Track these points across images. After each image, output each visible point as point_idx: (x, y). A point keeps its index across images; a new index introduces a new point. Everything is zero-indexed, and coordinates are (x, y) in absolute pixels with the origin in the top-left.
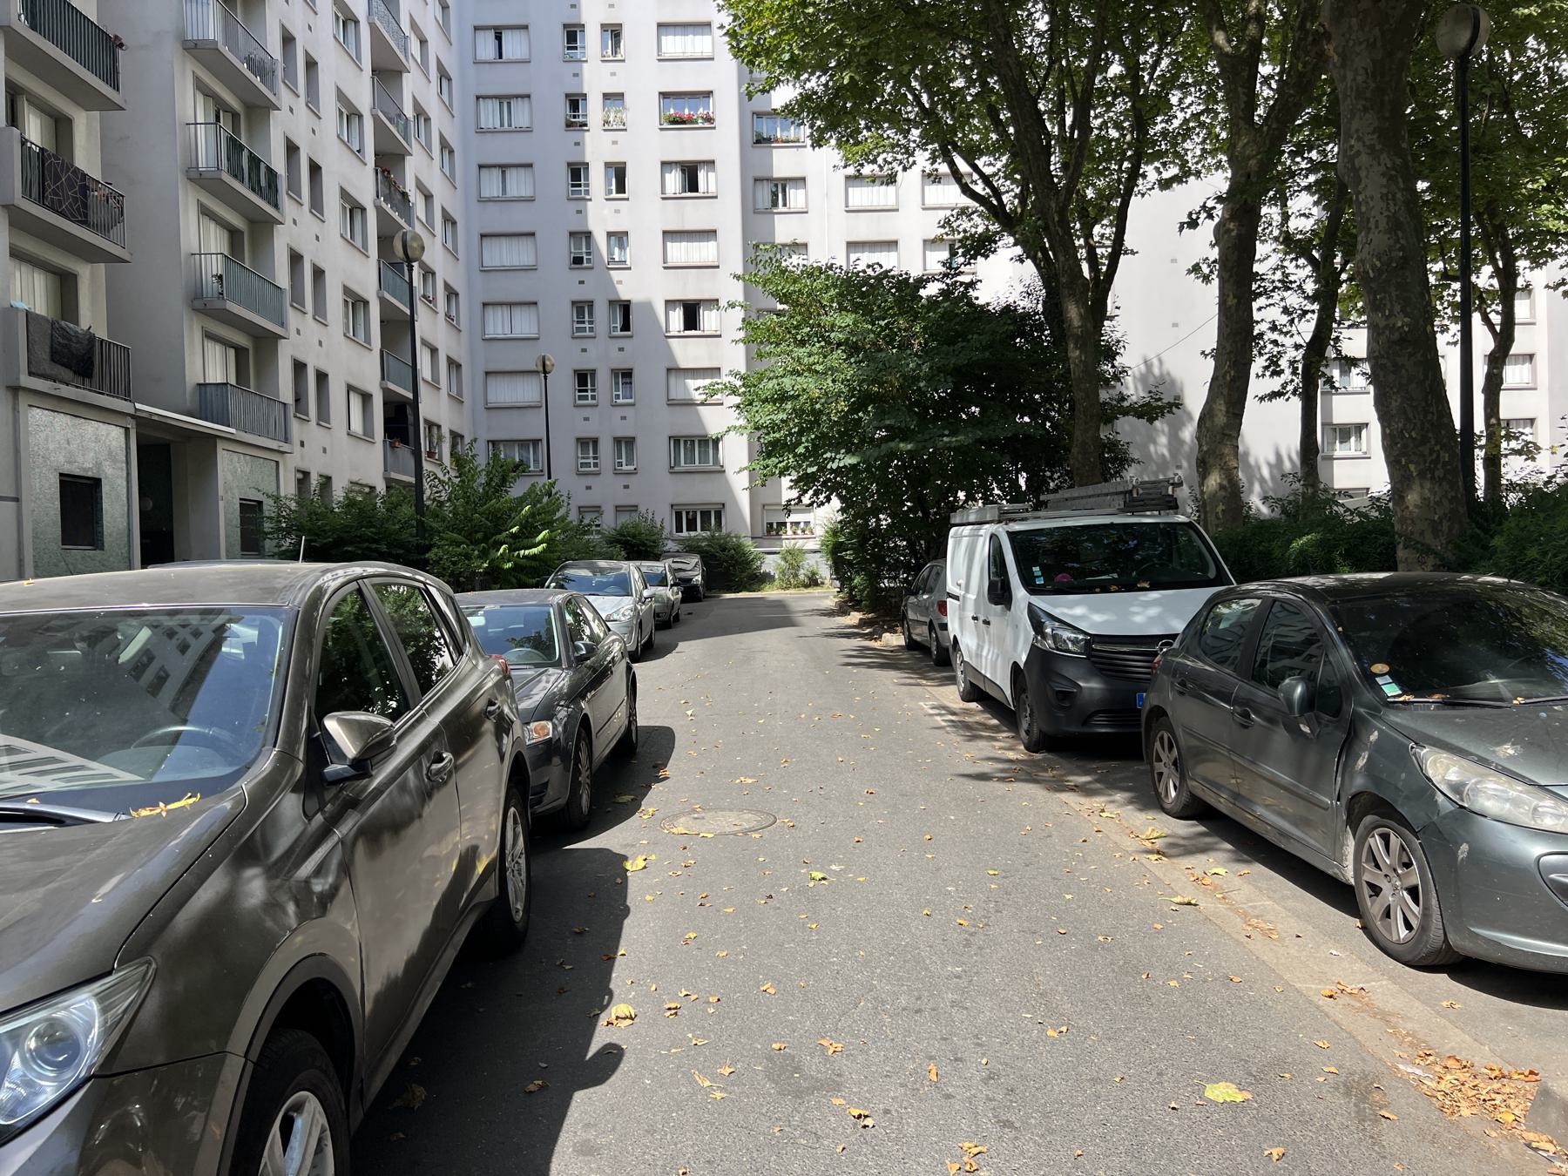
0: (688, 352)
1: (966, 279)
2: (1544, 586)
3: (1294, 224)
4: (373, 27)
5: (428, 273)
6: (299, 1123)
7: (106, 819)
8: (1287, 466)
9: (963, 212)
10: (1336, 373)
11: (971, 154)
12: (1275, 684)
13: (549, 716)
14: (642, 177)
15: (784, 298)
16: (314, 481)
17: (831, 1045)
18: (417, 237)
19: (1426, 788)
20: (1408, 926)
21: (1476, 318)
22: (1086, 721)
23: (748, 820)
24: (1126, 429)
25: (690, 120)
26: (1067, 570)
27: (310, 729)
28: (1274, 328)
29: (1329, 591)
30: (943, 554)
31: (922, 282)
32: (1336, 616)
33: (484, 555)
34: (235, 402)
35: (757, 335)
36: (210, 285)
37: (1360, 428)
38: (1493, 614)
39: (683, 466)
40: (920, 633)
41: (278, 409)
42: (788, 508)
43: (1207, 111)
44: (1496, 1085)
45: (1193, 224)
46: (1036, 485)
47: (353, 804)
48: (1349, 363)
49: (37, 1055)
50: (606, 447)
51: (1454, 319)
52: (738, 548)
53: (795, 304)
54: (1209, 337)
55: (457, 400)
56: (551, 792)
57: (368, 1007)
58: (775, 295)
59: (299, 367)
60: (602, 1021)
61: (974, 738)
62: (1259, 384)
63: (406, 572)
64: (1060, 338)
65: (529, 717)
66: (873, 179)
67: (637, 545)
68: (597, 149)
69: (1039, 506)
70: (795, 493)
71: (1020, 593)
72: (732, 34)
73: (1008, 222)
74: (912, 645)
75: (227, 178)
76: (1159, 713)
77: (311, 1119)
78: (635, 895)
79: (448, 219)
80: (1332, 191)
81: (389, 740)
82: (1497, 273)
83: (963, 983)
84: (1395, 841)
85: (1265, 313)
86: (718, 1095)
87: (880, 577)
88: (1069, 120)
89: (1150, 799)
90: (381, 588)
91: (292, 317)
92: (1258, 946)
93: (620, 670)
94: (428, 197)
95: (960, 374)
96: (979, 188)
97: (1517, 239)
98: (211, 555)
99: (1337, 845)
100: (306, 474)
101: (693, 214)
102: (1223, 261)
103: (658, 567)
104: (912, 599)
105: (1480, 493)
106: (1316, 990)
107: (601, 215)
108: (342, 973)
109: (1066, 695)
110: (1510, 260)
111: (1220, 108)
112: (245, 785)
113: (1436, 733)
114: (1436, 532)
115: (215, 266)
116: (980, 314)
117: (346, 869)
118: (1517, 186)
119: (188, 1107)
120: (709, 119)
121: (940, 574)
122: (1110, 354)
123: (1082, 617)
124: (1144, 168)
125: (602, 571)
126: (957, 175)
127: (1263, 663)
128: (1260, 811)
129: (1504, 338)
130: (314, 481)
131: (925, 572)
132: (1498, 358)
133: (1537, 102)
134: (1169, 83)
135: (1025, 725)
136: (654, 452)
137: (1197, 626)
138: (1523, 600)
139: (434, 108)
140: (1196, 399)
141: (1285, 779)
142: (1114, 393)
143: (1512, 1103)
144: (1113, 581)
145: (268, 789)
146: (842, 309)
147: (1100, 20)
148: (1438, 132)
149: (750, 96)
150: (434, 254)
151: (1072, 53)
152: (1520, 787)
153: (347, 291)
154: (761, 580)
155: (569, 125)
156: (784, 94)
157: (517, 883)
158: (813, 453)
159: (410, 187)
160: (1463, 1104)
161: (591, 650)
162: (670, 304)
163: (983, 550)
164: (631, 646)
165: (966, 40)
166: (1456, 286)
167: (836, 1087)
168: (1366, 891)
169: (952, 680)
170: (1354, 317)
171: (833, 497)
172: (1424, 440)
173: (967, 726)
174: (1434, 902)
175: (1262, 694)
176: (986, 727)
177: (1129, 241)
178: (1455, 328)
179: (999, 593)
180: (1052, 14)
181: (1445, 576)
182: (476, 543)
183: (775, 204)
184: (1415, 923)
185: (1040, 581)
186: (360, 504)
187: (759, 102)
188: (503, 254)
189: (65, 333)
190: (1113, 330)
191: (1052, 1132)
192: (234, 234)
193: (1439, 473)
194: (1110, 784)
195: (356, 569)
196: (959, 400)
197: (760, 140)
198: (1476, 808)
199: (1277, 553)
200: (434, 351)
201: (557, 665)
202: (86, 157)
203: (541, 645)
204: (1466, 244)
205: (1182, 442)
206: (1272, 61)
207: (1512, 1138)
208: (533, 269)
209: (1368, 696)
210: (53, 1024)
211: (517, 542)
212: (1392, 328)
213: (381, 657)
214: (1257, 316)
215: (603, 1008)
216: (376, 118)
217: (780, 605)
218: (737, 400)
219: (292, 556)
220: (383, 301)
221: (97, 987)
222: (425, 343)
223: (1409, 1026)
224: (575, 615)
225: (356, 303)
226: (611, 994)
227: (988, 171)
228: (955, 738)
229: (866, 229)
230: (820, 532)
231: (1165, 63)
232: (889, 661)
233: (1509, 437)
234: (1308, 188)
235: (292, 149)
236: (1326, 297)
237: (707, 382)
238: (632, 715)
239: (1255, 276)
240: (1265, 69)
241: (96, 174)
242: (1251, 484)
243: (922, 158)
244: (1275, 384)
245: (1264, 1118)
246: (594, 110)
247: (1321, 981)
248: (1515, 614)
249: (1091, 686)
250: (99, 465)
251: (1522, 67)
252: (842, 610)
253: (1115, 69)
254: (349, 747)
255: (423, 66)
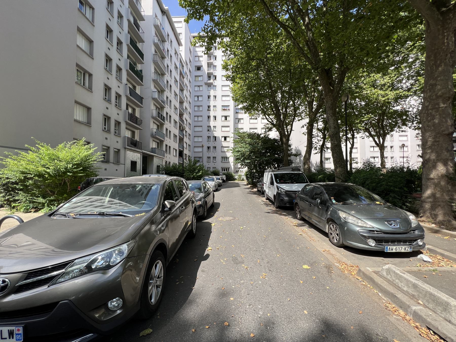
0: (224, 144)
1: (268, 134)
2: (359, 185)
3: (319, 127)
4: (180, 96)
5: (186, 132)
6: (158, 265)
7: (131, 216)
8: (318, 164)
9: (267, 124)
10: (326, 150)
11: (269, 115)
12: (316, 199)
13: (200, 201)
14: (218, 118)
15: (240, 136)
16: (168, 162)
17: (243, 256)
18: (184, 127)
19: (340, 218)
20: (337, 240)
21: (348, 142)
22: (285, 204)
23: (231, 218)
24: (292, 158)
25: (226, 110)
26: (283, 180)
27: (163, 203)
28: (316, 143)
29: (324, 185)
30: (263, 176)
31: (261, 134)
32: (325, 189)
33: (192, 174)
34: (157, 151)
35: (235, 142)
36: (154, 133)
37: (329, 158)
38: (351, 190)
39: (223, 161)
40: (260, 189)
41: (163, 151)
42: (239, 168)
43: (306, 109)
44: (351, 268)
45: (303, 127)
46: (278, 166)
47: (169, 215)
48: (328, 148)
49: (118, 254)
50: (212, 158)
51: (344, 142)
52: (231, 174)
53: (241, 137)
54: (306, 144)
55: (189, 151)
56: (200, 212)
57: (170, 246)
58: (238, 136)
59: (166, 145)
60: (207, 250)
61: (267, 206)
62: (313, 151)
63: (179, 178)
64: (282, 143)
65: (197, 201)
66: (254, 119)
67: (216, 173)
68: (212, 114)
69: (278, 169)
70: (240, 166)
71: (275, 183)
72: (233, 97)
73: (274, 125)
74: (258, 191)
75: (157, 117)
76: (297, 203)
77: (160, 265)
78: (213, 230)
79: (189, 124)
80: (325, 122)
81: (175, 205)
82: (351, 135)
83: (264, 246)
84: (334, 226)
85: (314, 140)
86: (224, 263)
87: (253, 180)
88: (284, 110)
89: (295, 217)
90: (175, 181)
91: (166, 138)
92: (312, 242)
93: (212, 193)
94: (187, 121)
95: (267, 149)
96: (270, 120)
97: (355, 129)
98: (152, 173)
99: (325, 226)
100: (167, 161)
101: (226, 123)
102: (308, 132)
103: (219, 177)
104: (258, 183)
105: (349, 170)
106: (321, 250)
107: (212, 124)
108: (166, 242)
109: (282, 200)
110: (353, 133)
111: (307, 109)
112: (152, 212)
113: (341, 209)
114: (342, 176)
115: (155, 130)
116: (270, 139)
117: (167, 226)
118: (354, 121)
119: (140, 262)
120: (229, 110)
121: (263, 180)
122: (290, 146)
123: (285, 188)
124: (295, 118)
125: (210, 177)
126: (267, 119)
127: (314, 196)
128: (313, 220)
129: (353, 145)
130: (168, 162)
131: (260, 179)
132: (352, 148)
133: (358, 109)
134: (300, 105)
135: (275, 204)
136: (219, 159)
137: (303, 190)
138: (356, 188)
139: (188, 108)
140: (303, 153)
141: (317, 215)
142: (290, 152)
143: (354, 271)
144: (290, 182)
145: (156, 212)
146: (248, 138)
147: (289, 95)
148: (342, 113)
149: (235, 107)
150: (187, 129)
151: (284, 100)
152: (355, 218)
153: (174, 134)
154: (235, 179)
155: (208, 110)
156: (241, 106)
157: (194, 227)
158: (243, 161)
159: (184, 119)
160: (346, 271)
161: (207, 190)
162: (222, 137)
163: (270, 176)
164: (214, 189)
165: (268, 98)
166: (345, 137)
167: (243, 263)
168: (330, 234)
169: (264, 197)
170: (329, 141)
171: (246, 167)
172: (340, 161)
173: (266, 204)
174: (341, 236)
175: (313, 201)
176: (270, 204)
177: (293, 129)
178: (345, 143)
179: (272, 183)
180: (282, 94)
181: (343, 183)
182: (191, 173)
183: (239, 122)
184: (338, 240)
185: (278, 182)
186: (174, 166)
187: (237, 107)
188: (197, 129)
189: (133, 140)
190: (290, 142)
191: (278, 272)
192: (158, 126)
193: (342, 166)
194: (289, 214)
195: (172, 178)
196: (266, 152)
197: (237, 113)
198: (348, 221)
199: (316, 178)
200: (186, 143)
201: (202, 192)
202: (137, 114)
203: (200, 189)
204: (346, 131)
205: (301, 160)
206: (316, 102)
207: (354, 277)
208: (202, 131)
209: (330, 202)
210: (120, 249)
211: (197, 173)
212: (335, 144)
213: (174, 191)
214: (313, 141)
215: (207, 248)
216: (179, 109)
217: (238, 183)
218: (232, 151)
219: (163, 174)
220: (179, 136)
221: (127, 243)
222: (185, 142)
223: (337, 257)
224: (205, 185)
225: (175, 136)
226: (208, 245)
227: (271, 118)
228: (265, 206)
229: (252, 126)
230: (244, 172)
231: (299, 102)
232: (255, 193)
233: (353, 161)
234: (321, 121)
235: (167, 113)
236: (324, 138)
237: (227, 149)
238: (214, 201)
239: (313, 135)
240: (314, 103)
241: (138, 117)
242: (312, 167)
243: (261, 116)
244: (316, 151)
245: (312, 272)
246: (212, 108)
247: (322, 249)
248: (354, 190)
249: (286, 198)
250: (137, 159)
251: (356, 103)
252: (247, 185)
253: (291, 103)
254: (169, 206)
255: (187, 102)
